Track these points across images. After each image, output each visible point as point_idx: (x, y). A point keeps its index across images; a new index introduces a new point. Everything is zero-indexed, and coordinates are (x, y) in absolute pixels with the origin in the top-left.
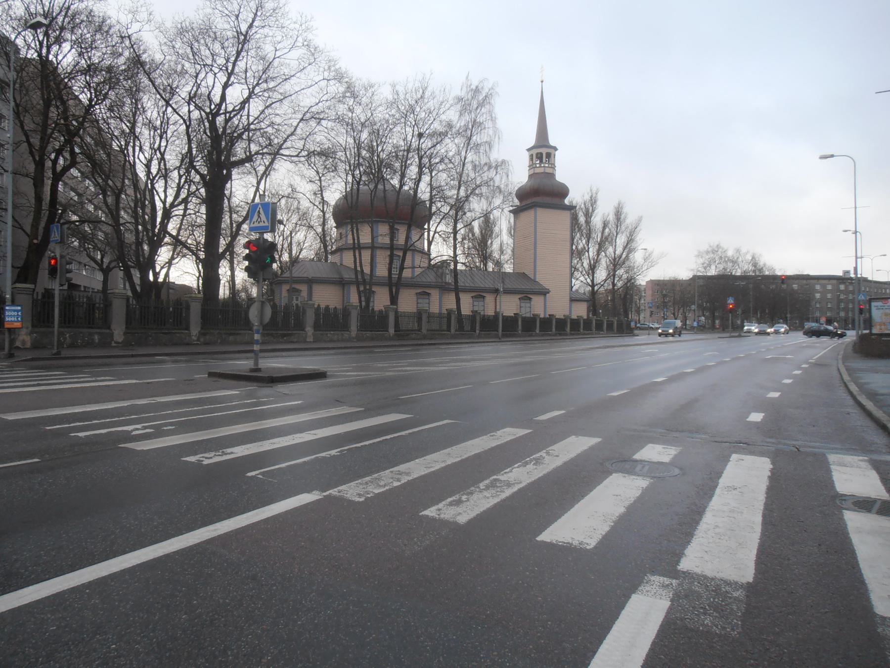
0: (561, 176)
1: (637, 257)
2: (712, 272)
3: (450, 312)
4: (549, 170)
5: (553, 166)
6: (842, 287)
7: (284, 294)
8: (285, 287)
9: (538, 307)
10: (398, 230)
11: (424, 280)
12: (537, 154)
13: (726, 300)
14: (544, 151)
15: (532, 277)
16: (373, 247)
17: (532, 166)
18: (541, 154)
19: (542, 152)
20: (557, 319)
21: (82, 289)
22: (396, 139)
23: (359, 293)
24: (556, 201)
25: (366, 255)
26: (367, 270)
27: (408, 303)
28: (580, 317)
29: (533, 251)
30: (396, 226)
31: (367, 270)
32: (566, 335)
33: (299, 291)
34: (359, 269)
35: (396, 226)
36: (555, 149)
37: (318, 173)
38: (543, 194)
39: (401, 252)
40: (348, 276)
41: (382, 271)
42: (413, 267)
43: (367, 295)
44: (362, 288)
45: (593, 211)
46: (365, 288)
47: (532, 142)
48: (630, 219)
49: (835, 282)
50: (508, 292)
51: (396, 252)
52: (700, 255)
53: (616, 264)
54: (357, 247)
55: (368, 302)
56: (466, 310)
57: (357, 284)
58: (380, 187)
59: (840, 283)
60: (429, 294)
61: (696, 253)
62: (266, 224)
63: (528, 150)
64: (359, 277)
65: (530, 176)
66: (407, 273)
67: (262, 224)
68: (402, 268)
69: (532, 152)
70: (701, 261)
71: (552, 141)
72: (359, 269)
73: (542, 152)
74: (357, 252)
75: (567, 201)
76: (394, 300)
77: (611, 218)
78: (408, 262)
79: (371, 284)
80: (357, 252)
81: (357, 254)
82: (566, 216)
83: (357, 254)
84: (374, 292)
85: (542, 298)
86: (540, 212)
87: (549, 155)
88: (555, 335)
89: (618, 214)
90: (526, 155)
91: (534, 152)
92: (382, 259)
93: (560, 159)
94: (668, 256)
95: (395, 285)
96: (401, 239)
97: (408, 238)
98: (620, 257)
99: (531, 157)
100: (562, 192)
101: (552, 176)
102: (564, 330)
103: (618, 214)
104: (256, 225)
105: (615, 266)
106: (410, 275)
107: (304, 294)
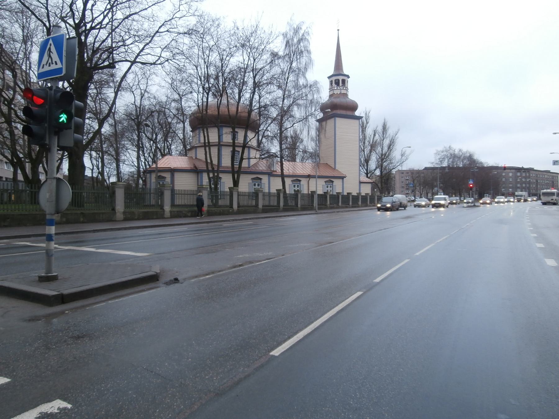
0: (353, 95)
1: (396, 154)
2: (445, 164)
3: (278, 191)
4: (343, 92)
5: (347, 90)
6: (519, 174)
7: (153, 180)
8: (154, 176)
9: (337, 187)
10: (237, 132)
11: (257, 169)
12: (336, 80)
13: (468, 183)
14: (341, 78)
15: (333, 166)
16: (220, 145)
17: (331, 89)
18: (339, 80)
19: (339, 79)
20: (353, 196)
21: (4, 179)
22: (237, 60)
23: (210, 178)
24: (349, 113)
25: (214, 150)
26: (215, 162)
27: (245, 185)
28: (367, 194)
29: (333, 148)
30: (236, 130)
31: (215, 162)
32: (358, 207)
33: (164, 178)
34: (209, 161)
35: (236, 130)
36: (348, 77)
37: (179, 94)
38: (340, 108)
39: (239, 150)
40: (202, 166)
41: (226, 162)
42: (249, 159)
43: (216, 181)
44: (211, 175)
45: (367, 123)
46: (214, 175)
47: (331, 72)
48: (391, 132)
49: (513, 171)
50: (320, 177)
51: (237, 149)
52: (437, 153)
53: (383, 158)
54: (207, 145)
55: (216, 185)
56: (290, 190)
57: (208, 172)
58: (224, 101)
59: (518, 171)
60: (261, 179)
61: (435, 152)
62: (59, 66)
63: (329, 78)
64: (210, 167)
65: (331, 96)
66: (245, 164)
67: (53, 67)
68: (242, 159)
69: (331, 79)
70: (439, 157)
71: (346, 72)
72: (209, 161)
73: (339, 79)
74: (207, 149)
75: (357, 113)
76: (236, 183)
77: (380, 129)
78: (246, 155)
79: (218, 172)
80: (207, 149)
81: (208, 150)
82: (356, 122)
83: (208, 150)
84: (220, 178)
85: (341, 180)
86: (339, 121)
87: (344, 81)
88: (342, 207)
89: (385, 128)
90: (328, 82)
91: (334, 79)
92: (227, 153)
93: (350, 83)
94: (418, 154)
95: (236, 173)
96: (240, 139)
97: (246, 136)
98: (385, 154)
99: (331, 83)
100: (353, 107)
101: (346, 95)
102: (349, 205)
103: (385, 128)
104: (47, 68)
105: (382, 160)
106: (247, 166)
107: (168, 180)
